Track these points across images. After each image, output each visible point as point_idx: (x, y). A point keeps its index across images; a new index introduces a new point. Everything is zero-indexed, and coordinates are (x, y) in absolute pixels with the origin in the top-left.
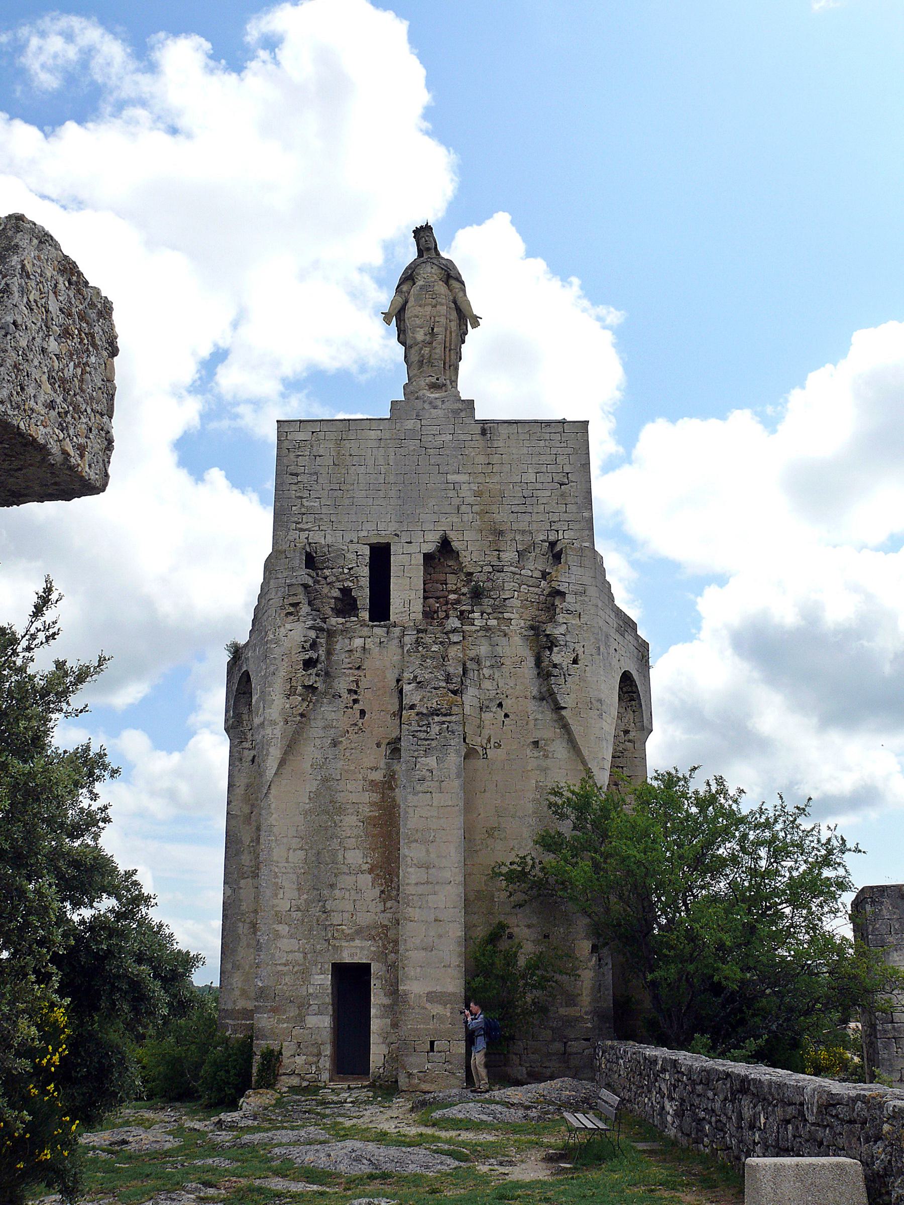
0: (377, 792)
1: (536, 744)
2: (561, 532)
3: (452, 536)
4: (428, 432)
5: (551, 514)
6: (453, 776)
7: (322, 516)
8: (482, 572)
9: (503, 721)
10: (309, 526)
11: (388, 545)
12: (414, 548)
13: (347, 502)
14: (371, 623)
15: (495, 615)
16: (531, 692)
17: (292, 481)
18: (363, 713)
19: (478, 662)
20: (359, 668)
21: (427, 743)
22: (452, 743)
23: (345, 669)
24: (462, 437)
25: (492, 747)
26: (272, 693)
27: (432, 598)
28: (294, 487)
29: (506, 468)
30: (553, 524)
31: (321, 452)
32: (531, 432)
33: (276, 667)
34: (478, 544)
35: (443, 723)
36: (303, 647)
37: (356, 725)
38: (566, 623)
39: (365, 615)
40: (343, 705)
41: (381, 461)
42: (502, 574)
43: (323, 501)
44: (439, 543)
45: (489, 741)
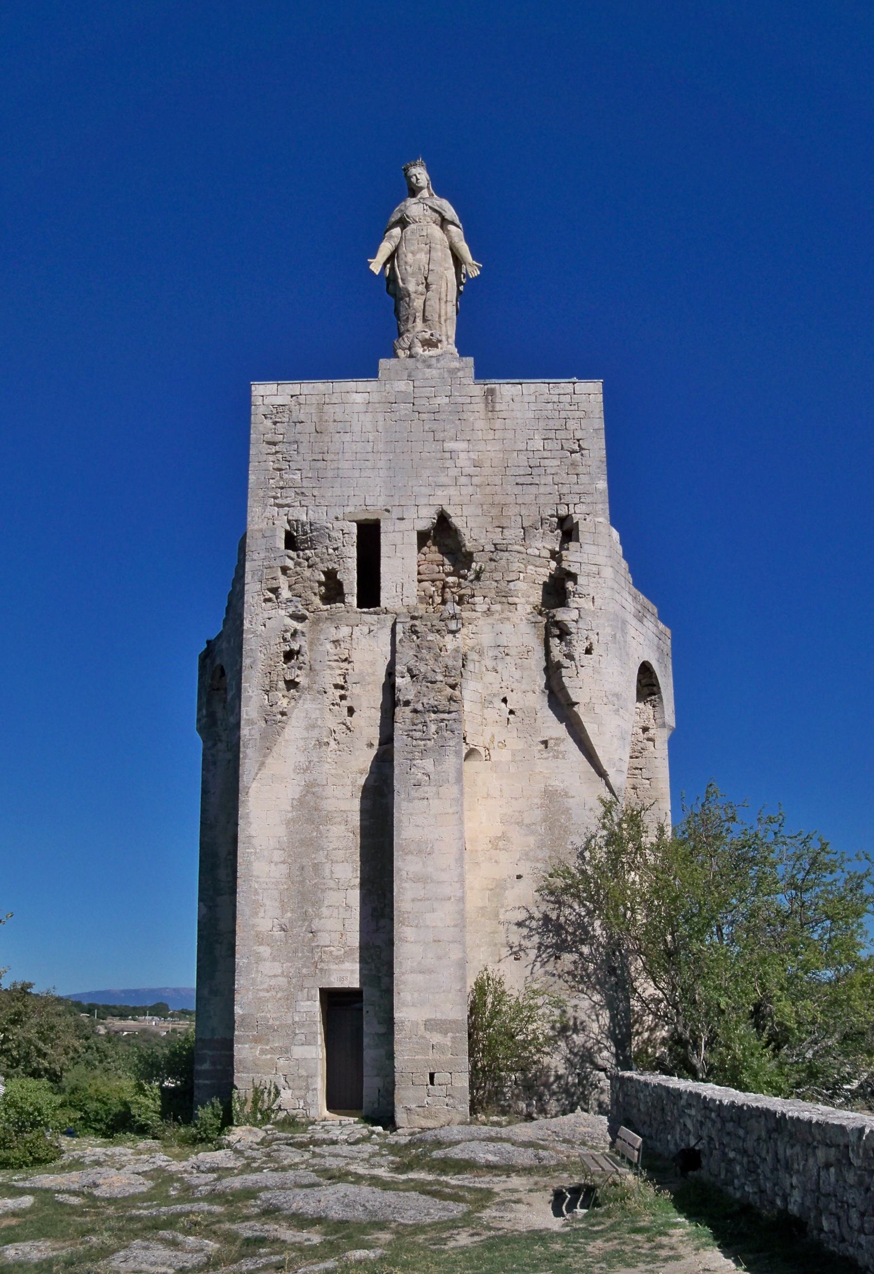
1: (545, 743)
2: (571, 506)
3: (450, 510)
13: (330, 474)
18: (351, 711)
21: (423, 743)
24: (460, 400)
27: (427, 581)
28: (271, 458)
31: (302, 417)
34: (478, 519)
39: (352, 600)
40: (328, 702)
41: (369, 427)
42: (506, 554)
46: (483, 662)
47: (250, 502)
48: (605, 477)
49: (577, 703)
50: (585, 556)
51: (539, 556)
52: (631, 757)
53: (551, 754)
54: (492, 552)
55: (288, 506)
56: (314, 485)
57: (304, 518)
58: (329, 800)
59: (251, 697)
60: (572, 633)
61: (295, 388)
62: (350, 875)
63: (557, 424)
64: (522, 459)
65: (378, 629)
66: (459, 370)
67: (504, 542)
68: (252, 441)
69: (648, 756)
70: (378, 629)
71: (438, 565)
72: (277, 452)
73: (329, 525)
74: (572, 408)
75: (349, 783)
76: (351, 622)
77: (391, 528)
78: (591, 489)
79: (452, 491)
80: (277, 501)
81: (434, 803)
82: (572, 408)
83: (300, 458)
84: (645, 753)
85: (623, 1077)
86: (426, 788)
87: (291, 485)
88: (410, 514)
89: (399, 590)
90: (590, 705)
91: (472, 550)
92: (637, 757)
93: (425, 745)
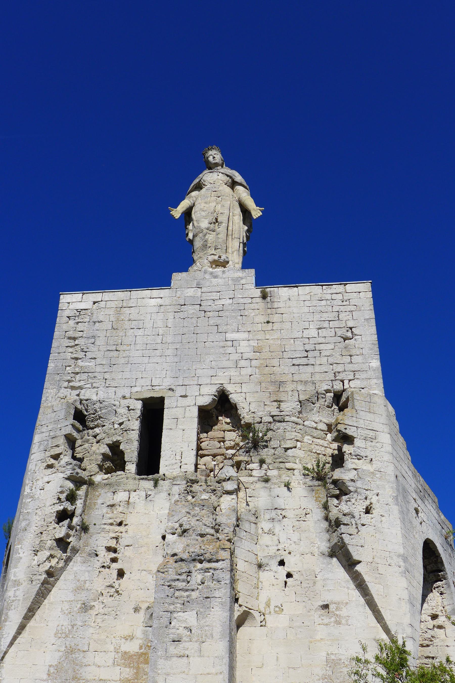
0: (130, 667)
1: (326, 607)
2: (346, 382)
3: (230, 388)
4: (208, 298)
5: (335, 365)
6: (217, 635)
7: (96, 374)
8: (261, 422)
9: (286, 583)
10: (82, 383)
11: (162, 400)
12: (189, 401)
13: (122, 361)
14: (139, 477)
15: (276, 465)
16: (318, 548)
17: (70, 344)
18: (121, 574)
19: (256, 515)
20: (120, 524)
21: (186, 594)
22: (217, 594)
23: (105, 524)
24: (242, 301)
25: (272, 611)
26: (20, 551)
27: (208, 455)
28: (70, 350)
29: (287, 325)
30: (337, 374)
31: (101, 318)
32: (312, 294)
33: (28, 522)
34: (256, 395)
35: (207, 570)
36: (59, 499)
37: (113, 587)
38: (356, 469)
39: (131, 467)
40: (99, 564)
41: (160, 324)
42: (284, 424)
43: (98, 361)
44: (215, 396)
45: (268, 605)
46: (260, 525)
47: (46, 385)
48: (378, 357)
49: (359, 562)
50: (362, 421)
51: (316, 429)
52: (422, 646)
53: (333, 619)
54: (270, 423)
55: (80, 388)
56: (106, 370)
57: (94, 398)
58: (88, 668)
59: (21, 558)
60: (351, 492)
61: (97, 296)
63: (332, 316)
65: (155, 494)
66: (242, 278)
67: (282, 414)
68: (55, 337)
69: (439, 644)
70: (155, 494)
71: (219, 442)
72: (76, 345)
73: (117, 403)
74: (345, 303)
75: (112, 648)
76: (130, 487)
77: (174, 404)
78: (365, 367)
80: (71, 384)
81: (195, 661)
82: (345, 303)
83: (96, 349)
84: (435, 641)
86: (187, 645)
87: (86, 370)
88: (193, 391)
89: (178, 457)
90: (373, 565)
91: (251, 421)
92: (428, 646)
93: (188, 597)
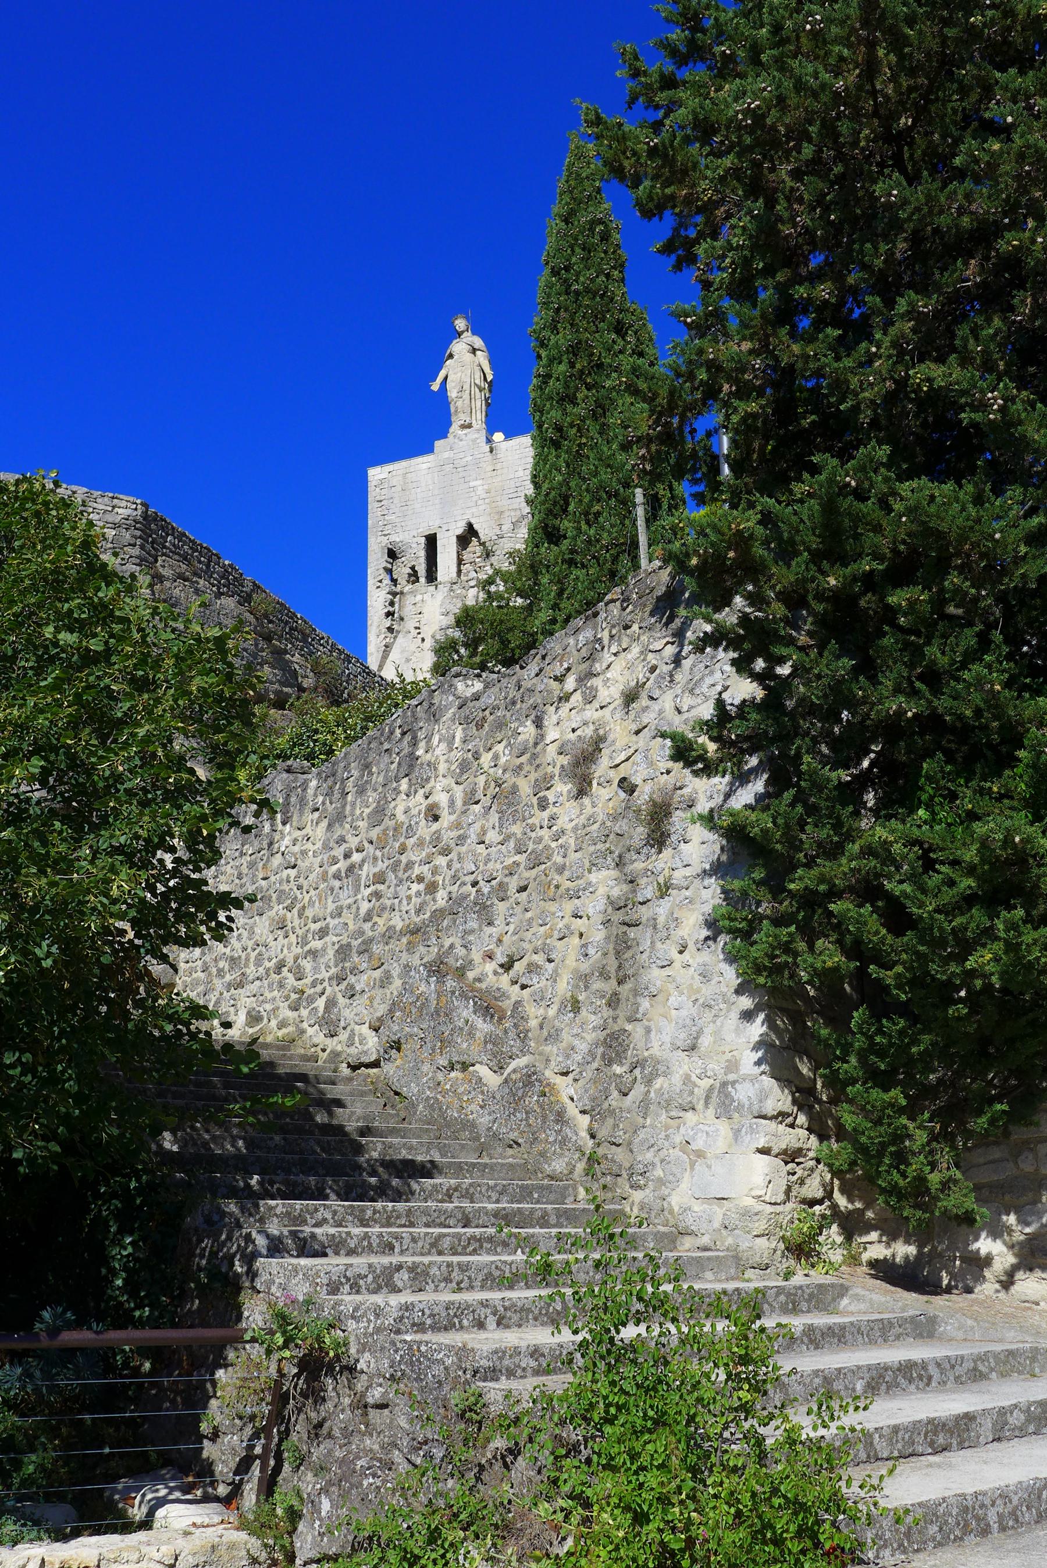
3: (473, 521)
12: (450, 533)
18: (423, 640)
39: (422, 580)
62: (521, 473)
64: (512, 484)
79: (474, 510)
85: (188, 876)
88: (452, 526)
91: (459, 605)
